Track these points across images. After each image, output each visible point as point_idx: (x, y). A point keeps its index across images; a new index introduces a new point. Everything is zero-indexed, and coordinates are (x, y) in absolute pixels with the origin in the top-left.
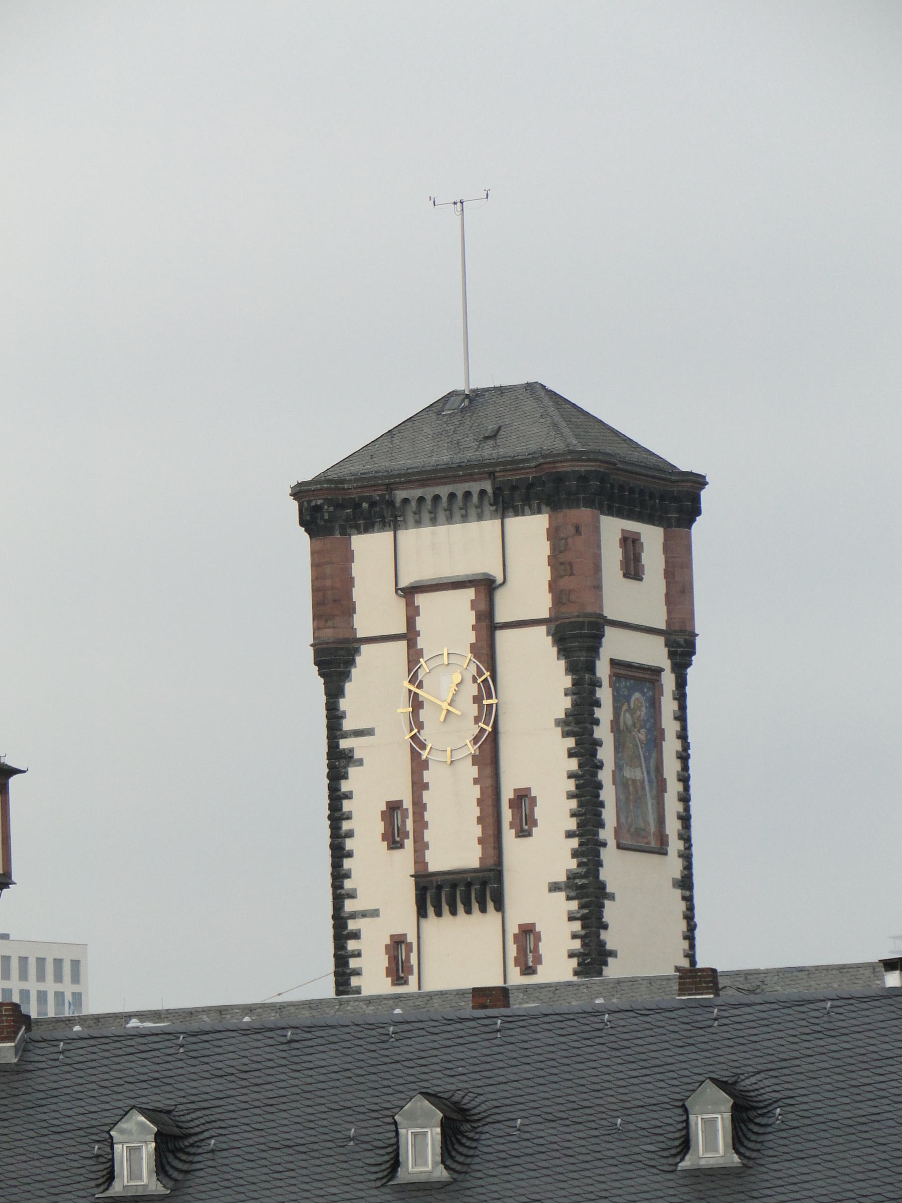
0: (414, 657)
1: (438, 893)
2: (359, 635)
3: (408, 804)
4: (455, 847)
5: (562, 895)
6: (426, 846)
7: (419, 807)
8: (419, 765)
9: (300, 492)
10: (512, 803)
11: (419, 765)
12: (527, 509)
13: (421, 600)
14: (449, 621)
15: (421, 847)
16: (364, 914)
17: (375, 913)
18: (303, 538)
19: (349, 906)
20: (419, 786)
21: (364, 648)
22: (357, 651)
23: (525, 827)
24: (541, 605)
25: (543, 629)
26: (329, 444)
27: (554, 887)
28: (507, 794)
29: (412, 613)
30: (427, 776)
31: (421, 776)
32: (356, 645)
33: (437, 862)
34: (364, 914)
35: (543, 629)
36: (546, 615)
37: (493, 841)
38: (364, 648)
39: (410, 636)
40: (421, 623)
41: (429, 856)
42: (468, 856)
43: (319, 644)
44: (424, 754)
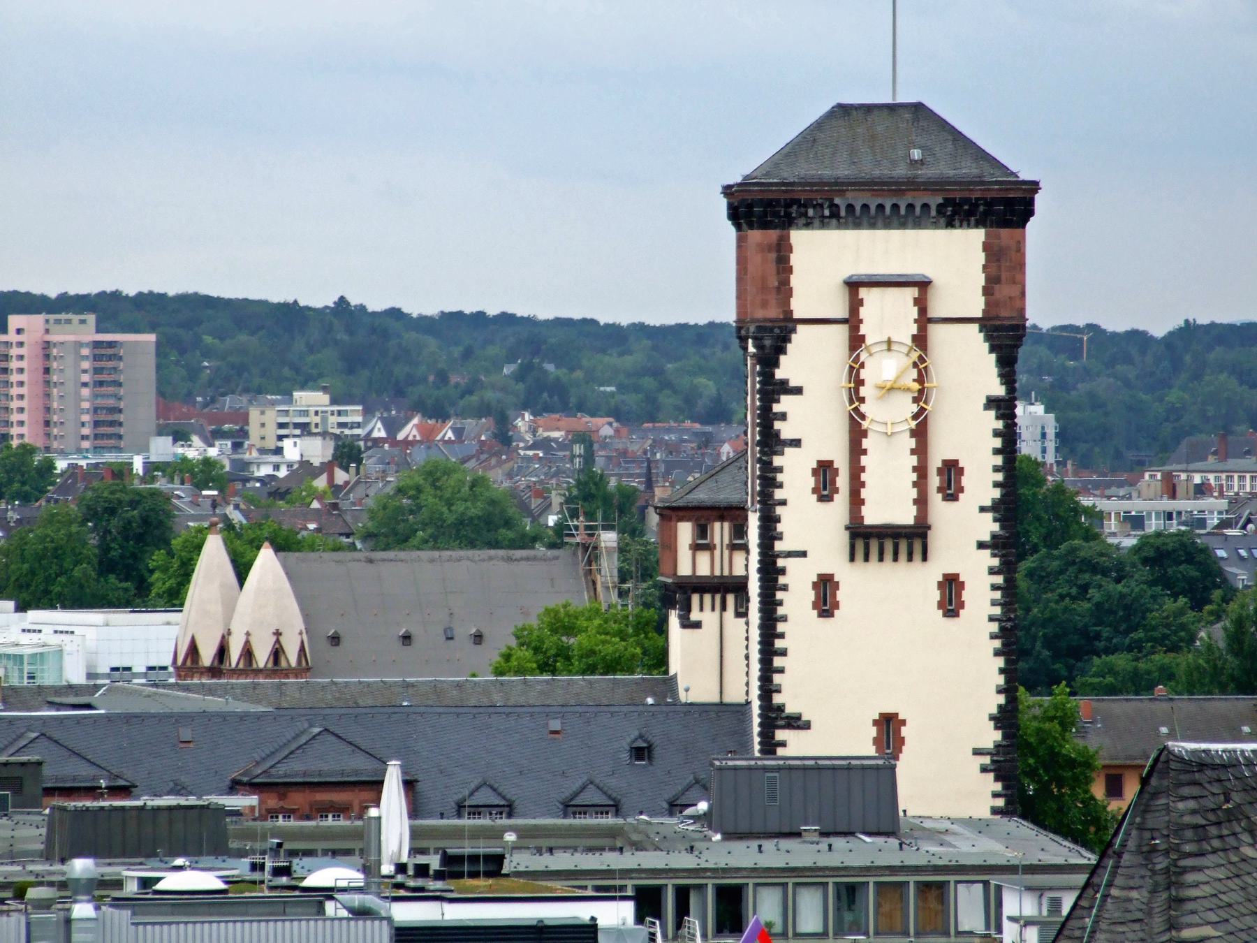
0: (856, 341)
1: (867, 540)
2: (796, 315)
3: (935, 498)
4: (889, 503)
5: (988, 552)
6: (862, 502)
7: (856, 471)
8: (857, 433)
9: (728, 191)
10: (940, 471)
11: (857, 433)
12: (965, 223)
13: (863, 293)
14: (888, 315)
15: (856, 501)
16: (790, 554)
17: (803, 554)
18: (730, 231)
19: (779, 546)
20: (856, 450)
21: (800, 327)
22: (794, 330)
23: (952, 491)
24: (976, 306)
25: (976, 327)
26: (747, 159)
27: (981, 545)
28: (935, 463)
29: (855, 304)
30: (865, 443)
31: (860, 444)
32: (790, 325)
33: (872, 516)
34: (790, 554)
35: (976, 327)
36: (979, 315)
37: (921, 502)
38: (800, 327)
39: (853, 321)
40: (863, 312)
41: (865, 511)
42: (905, 515)
43: (990, 319)
44: (865, 424)
